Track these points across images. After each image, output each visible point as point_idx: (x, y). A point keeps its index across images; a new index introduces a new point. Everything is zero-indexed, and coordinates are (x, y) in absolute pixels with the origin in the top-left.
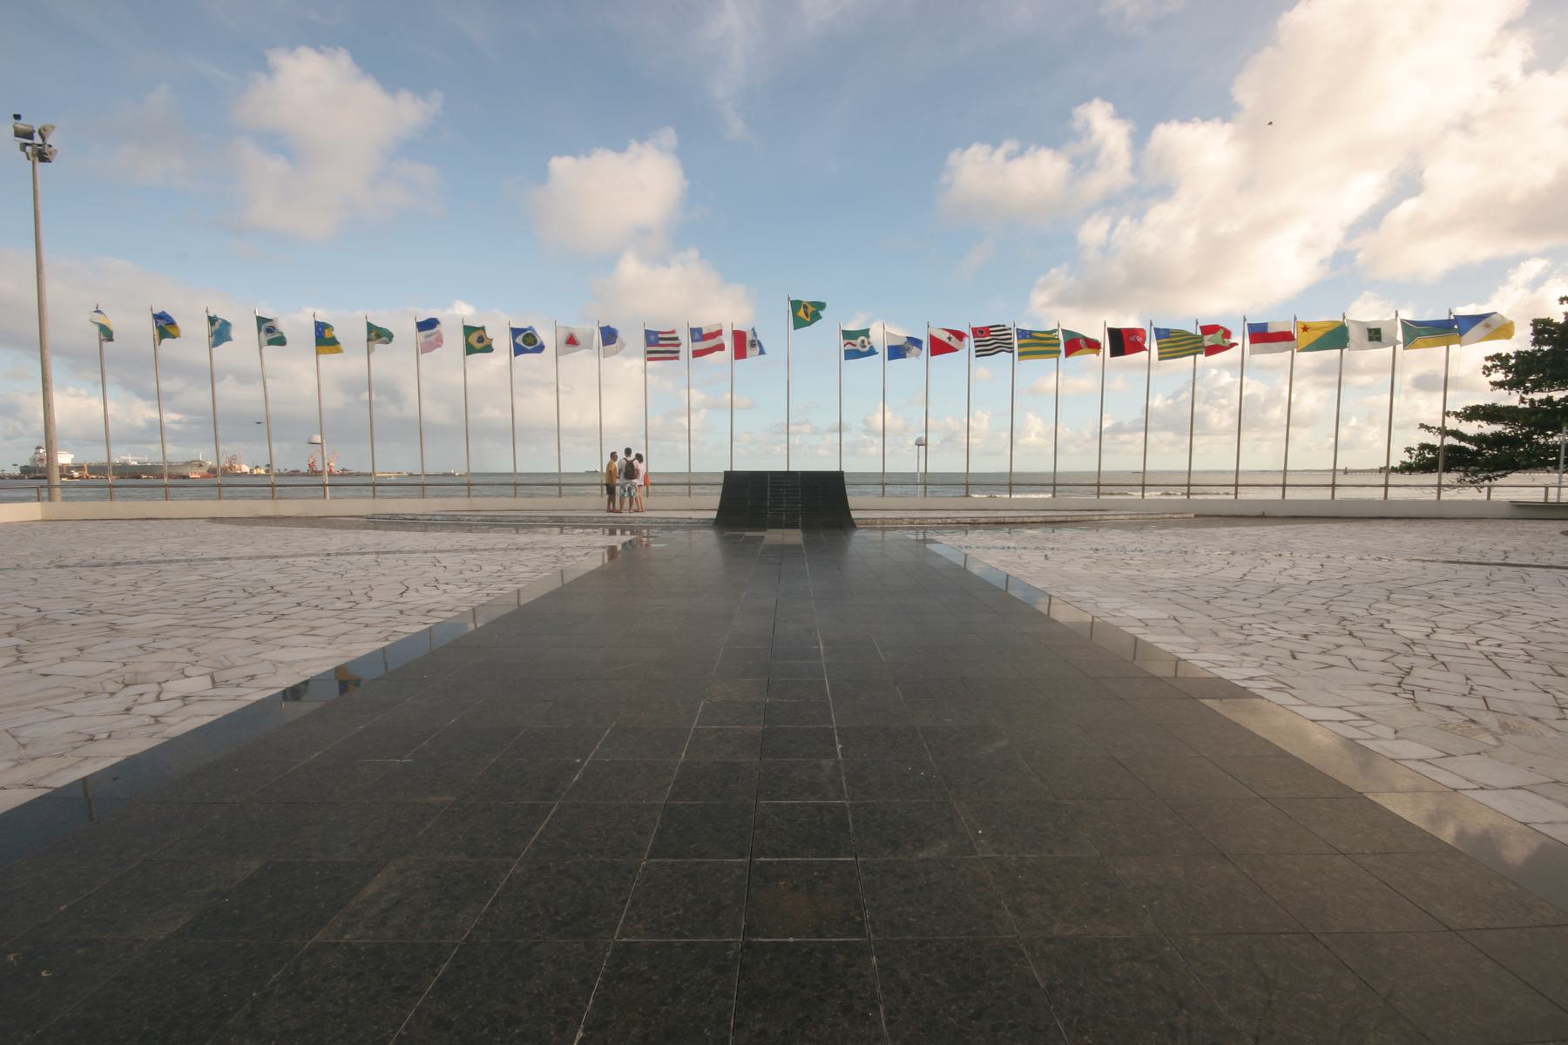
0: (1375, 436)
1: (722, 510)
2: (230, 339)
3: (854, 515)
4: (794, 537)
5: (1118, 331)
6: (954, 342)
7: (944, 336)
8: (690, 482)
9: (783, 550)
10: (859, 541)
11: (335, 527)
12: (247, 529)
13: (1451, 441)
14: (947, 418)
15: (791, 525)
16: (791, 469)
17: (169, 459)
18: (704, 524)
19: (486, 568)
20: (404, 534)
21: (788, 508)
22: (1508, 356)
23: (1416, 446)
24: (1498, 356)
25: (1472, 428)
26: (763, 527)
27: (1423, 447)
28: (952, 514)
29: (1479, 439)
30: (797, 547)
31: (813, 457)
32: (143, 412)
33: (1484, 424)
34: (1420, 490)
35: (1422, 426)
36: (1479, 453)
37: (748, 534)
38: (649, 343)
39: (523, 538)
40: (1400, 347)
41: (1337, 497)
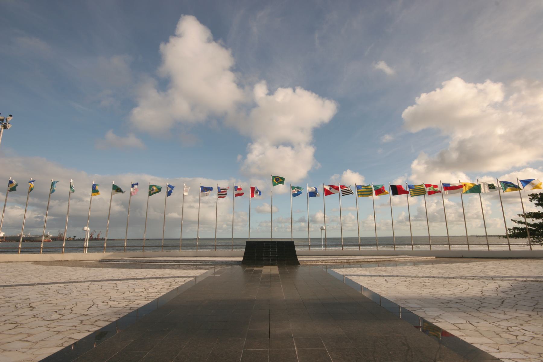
0: (500, 222)
1: (246, 256)
2: (435, 91)
3: (299, 259)
4: (274, 270)
5: (395, 186)
6: (333, 190)
7: (328, 188)
8: (229, 244)
9: (270, 277)
10: (300, 270)
11: (81, 266)
12: (45, 267)
13: (524, 226)
14: (350, 217)
15: (273, 264)
16: (235, 237)
17: (450, 234)
18: (238, 263)
19: (137, 290)
20: (110, 270)
21: (271, 254)
22: (537, 195)
23: (512, 228)
24: (532, 195)
25: (530, 221)
26: (262, 265)
27: (515, 228)
28: (353, 257)
29: (535, 225)
30: (275, 276)
31: (281, 233)
32: (31, 214)
33: (534, 219)
34: (521, 245)
35: (512, 220)
36: (536, 230)
37: (255, 269)
38: (219, 192)
39: (159, 272)
40: (501, 191)
41: (451, 249)
